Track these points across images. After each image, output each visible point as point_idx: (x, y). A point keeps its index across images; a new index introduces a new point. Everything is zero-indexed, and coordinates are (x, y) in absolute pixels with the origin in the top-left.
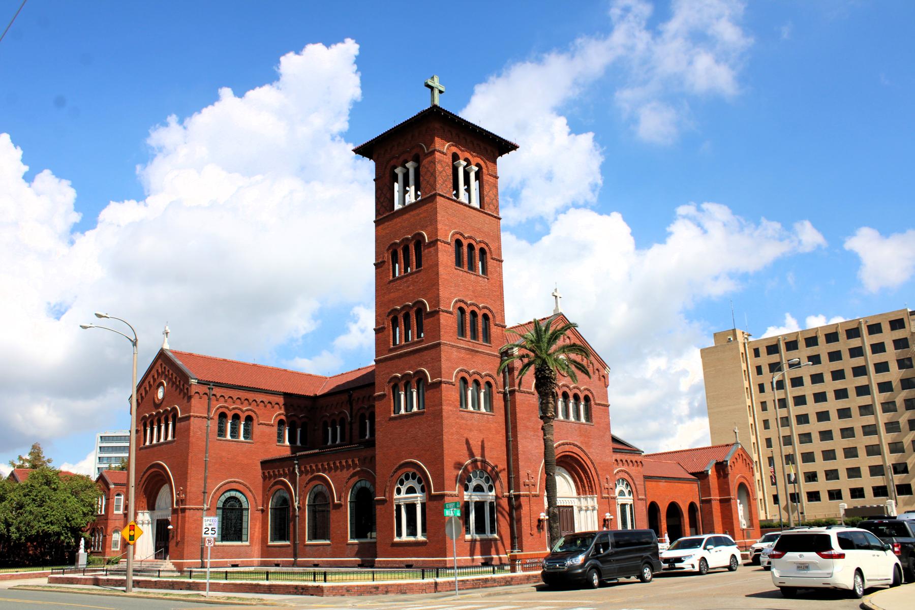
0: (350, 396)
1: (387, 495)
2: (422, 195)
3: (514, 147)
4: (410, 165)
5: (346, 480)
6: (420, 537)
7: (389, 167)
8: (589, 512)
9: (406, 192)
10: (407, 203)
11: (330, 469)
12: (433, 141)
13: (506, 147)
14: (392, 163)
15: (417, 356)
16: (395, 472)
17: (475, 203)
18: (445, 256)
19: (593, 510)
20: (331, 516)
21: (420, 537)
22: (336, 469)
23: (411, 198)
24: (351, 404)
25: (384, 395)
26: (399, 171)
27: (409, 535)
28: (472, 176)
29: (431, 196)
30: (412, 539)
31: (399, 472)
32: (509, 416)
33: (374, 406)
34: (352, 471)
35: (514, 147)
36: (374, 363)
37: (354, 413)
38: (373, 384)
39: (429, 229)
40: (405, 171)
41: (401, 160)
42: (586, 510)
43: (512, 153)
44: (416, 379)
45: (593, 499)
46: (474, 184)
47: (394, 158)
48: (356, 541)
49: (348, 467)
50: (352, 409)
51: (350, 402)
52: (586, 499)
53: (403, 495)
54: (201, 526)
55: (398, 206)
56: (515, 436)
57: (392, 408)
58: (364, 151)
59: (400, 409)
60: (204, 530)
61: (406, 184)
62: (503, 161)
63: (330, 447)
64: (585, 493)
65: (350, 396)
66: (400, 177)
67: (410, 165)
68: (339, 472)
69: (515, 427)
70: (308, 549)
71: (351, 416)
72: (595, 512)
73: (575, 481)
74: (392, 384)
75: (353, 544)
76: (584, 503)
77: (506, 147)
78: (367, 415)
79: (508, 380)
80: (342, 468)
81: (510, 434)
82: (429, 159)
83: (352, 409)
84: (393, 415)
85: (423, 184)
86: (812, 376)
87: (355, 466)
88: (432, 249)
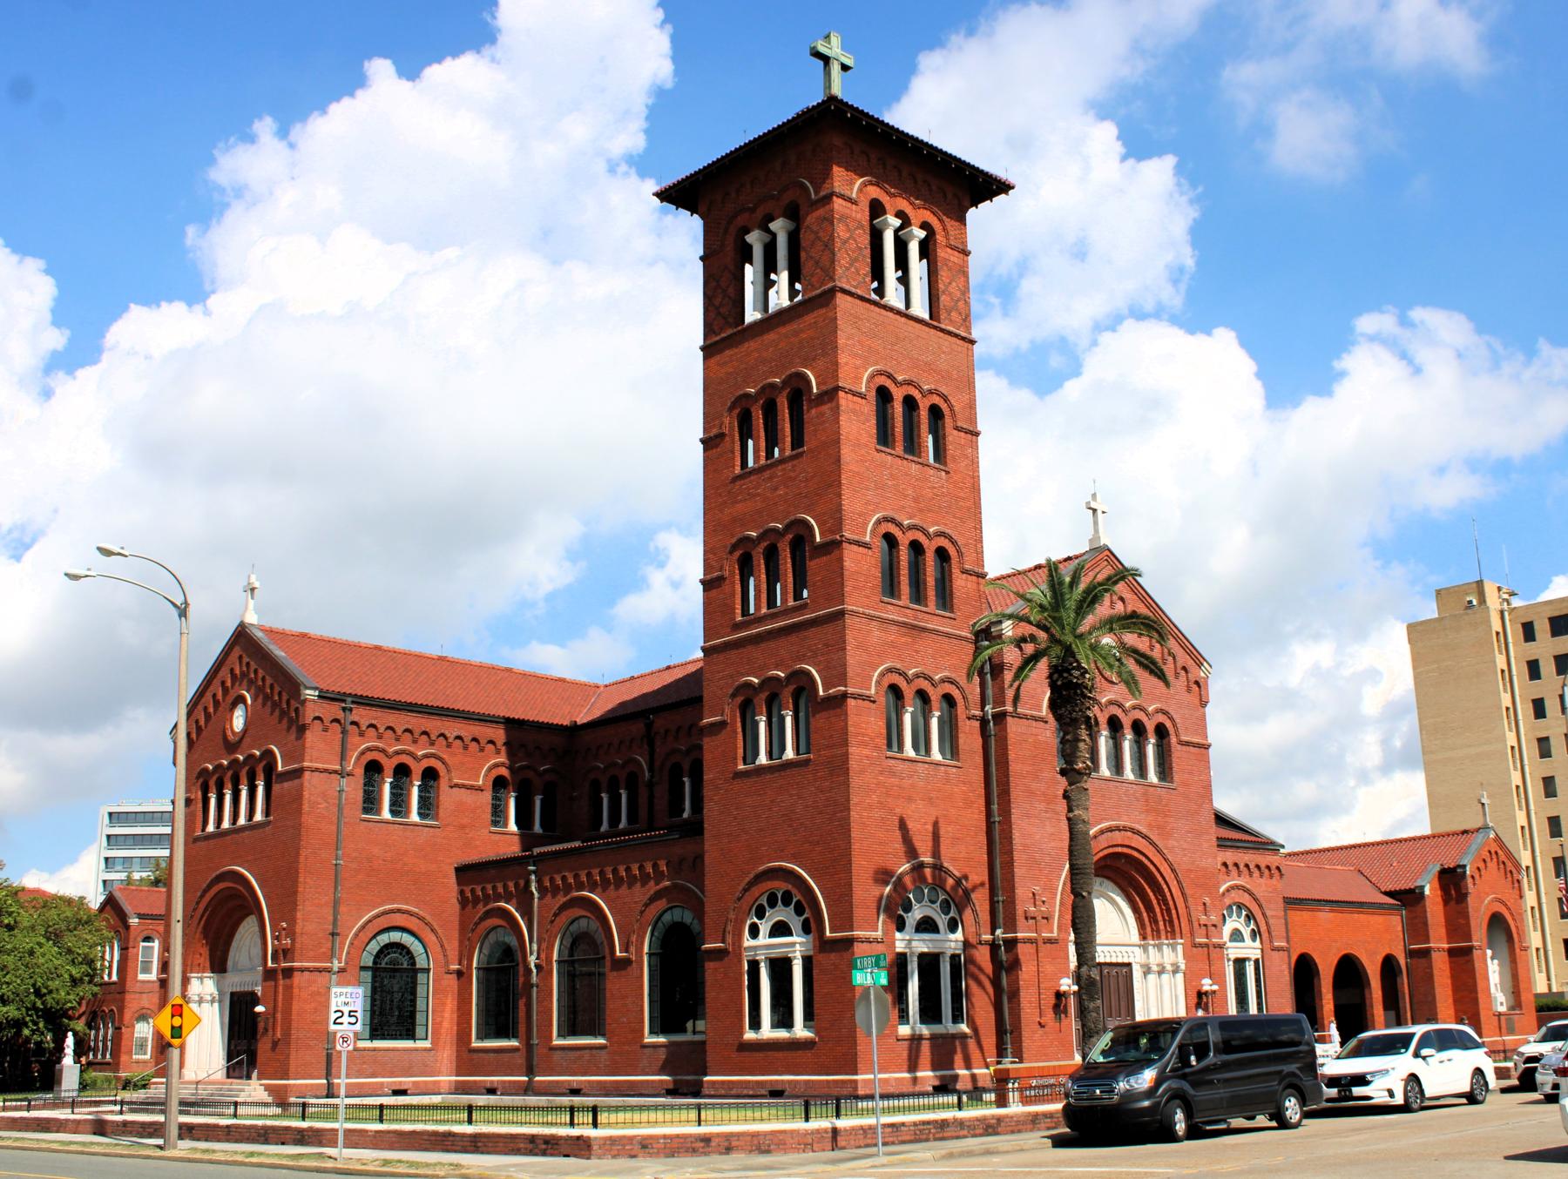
0: (649, 726)
2: (805, 291)
3: (1003, 187)
4: (779, 226)
5: (640, 907)
6: (800, 1031)
7: (733, 230)
8: (1165, 977)
9: (769, 284)
10: (772, 308)
11: (605, 884)
13: (986, 187)
15: (793, 638)
16: (746, 890)
17: (920, 308)
18: (855, 422)
19: (1175, 972)
20: (609, 986)
21: (800, 1031)
22: (619, 882)
23: (780, 298)
25: (723, 724)
26: (755, 239)
28: (914, 249)
29: (824, 293)
30: (782, 1034)
31: (756, 891)
33: (700, 748)
34: (652, 888)
35: (1003, 187)
36: (701, 654)
37: (657, 763)
38: (700, 699)
39: (820, 363)
40: (767, 238)
41: (759, 214)
42: (1160, 973)
43: (1000, 199)
44: (792, 688)
46: (918, 268)
48: (662, 1039)
49: (645, 879)
51: (649, 739)
52: (1159, 947)
53: (763, 939)
55: (752, 315)
56: (1006, 812)
57: (740, 752)
58: (678, 195)
59: (756, 754)
60: (333, 1016)
61: (770, 266)
62: (978, 216)
65: (649, 726)
66: (758, 253)
68: (624, 890)
70: (557, 1055)
71: (651, 770)
72: (1180, 976)
74: (739, 699)
75: (655, 1046)
76: (1154, 957)
77: (986, 187)
78: (686, 766)
79: (990, 692)
82: (821, 212)
85: (807, 267)
87: (659, 876)
88: (826, 408)
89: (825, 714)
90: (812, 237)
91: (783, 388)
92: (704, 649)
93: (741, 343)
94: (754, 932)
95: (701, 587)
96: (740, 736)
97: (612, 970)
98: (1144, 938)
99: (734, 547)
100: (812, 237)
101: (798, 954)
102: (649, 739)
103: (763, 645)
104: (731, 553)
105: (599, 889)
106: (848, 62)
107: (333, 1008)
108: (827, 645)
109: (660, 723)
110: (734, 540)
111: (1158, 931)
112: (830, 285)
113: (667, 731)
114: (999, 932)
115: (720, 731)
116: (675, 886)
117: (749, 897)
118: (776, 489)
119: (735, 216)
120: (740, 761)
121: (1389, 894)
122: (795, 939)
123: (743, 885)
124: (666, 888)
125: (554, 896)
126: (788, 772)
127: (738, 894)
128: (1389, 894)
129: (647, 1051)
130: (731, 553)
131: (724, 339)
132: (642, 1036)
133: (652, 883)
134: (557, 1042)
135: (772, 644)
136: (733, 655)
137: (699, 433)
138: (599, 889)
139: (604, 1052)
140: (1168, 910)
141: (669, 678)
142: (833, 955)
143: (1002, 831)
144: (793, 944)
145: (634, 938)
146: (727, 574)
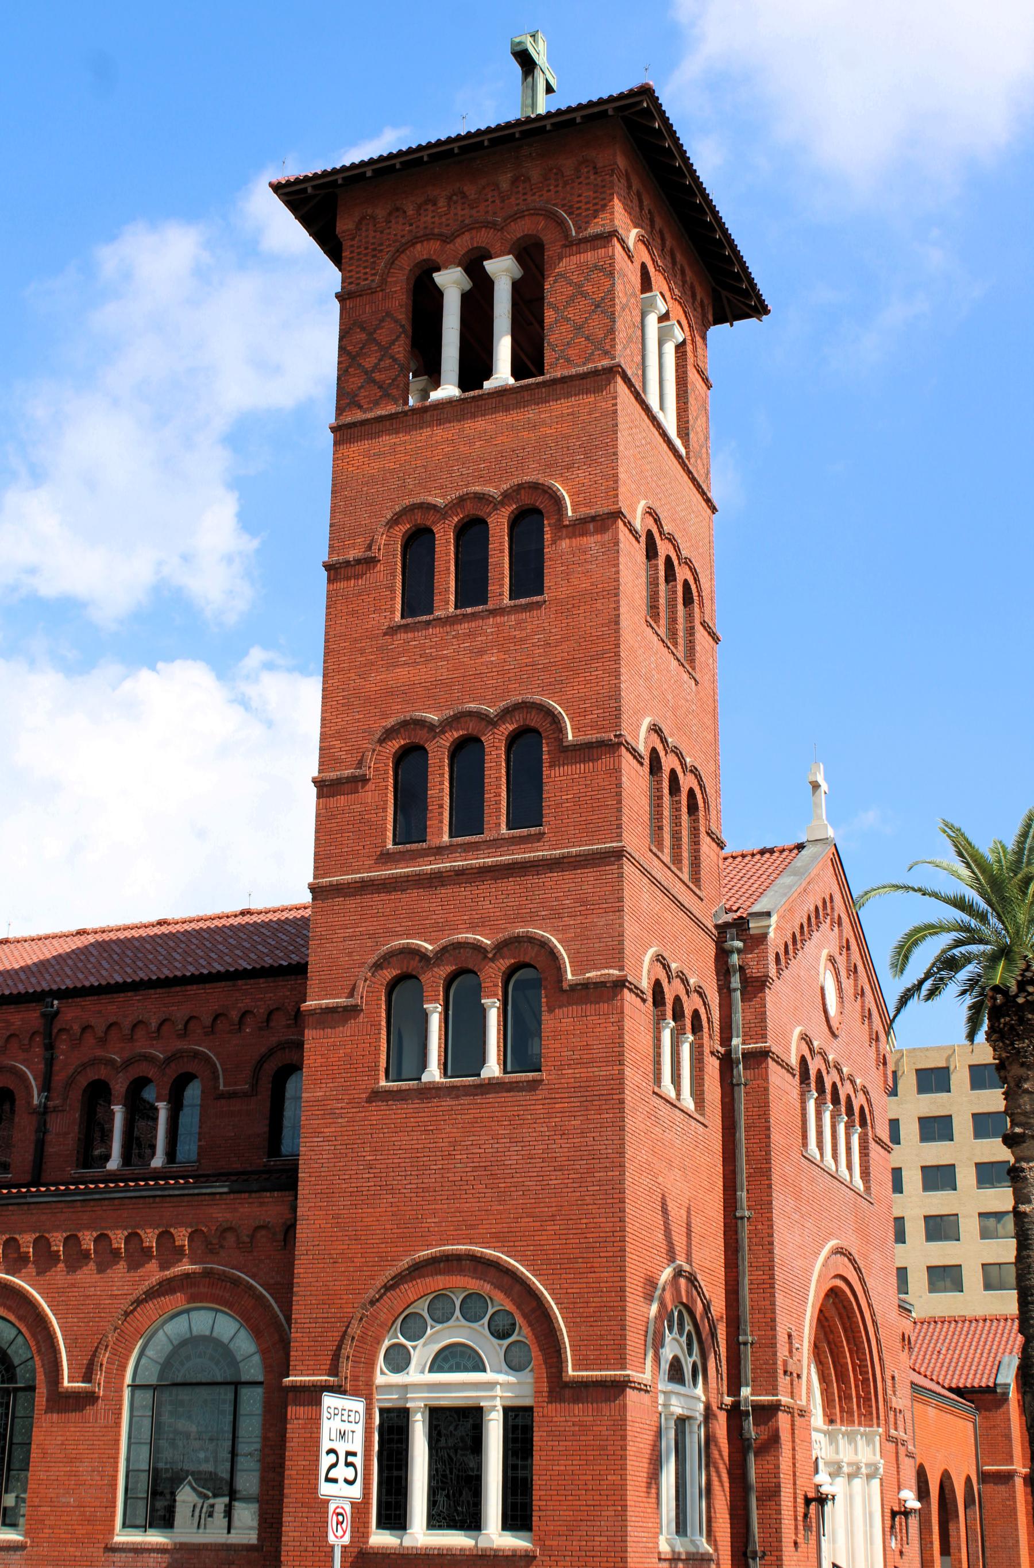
0: (50, 1018)
1: (100, 1377)
5: (125, 1305)
6: (495, 1535)
7: (406, 264)
8: (857, 1482)
11: (46, 1259)
12: (602, 206)
14: (422, 251)
15: (510, 885)
16: (388, 1288)
19: (870, 1477)
20: (37, 1437)
21: (495, 1535)
22: (77, 1258)
24: (50, 1047)
25: (351, 1012)
27: (436, 1520)
29: (595, 373)
30: (456, 1540)
31: (409, 1290)
32: (742, 1135)
33: (300, 1045)
34: (153, 1274)
36: (307, 898)
37: (60, 1078)
38: (300, 970)
39: (581, 475)
41: (463, 244)
42: (851, 1477)
44: (504, 963)
45: (869, 1442)
47: (428, 237)
49: (138, 1256)
50: (50, 1062)
51: (49, 1036)
52: (851, 1437)
53: (416, 1374)
54: (316, 1442)
56: (764, 1205)
57: (383, 1063)
59: (424, 1065)
60: (326, 1461)
63: (157, 1175)
64: (847, 1416)
65: (50, 1018)
67: (502, 269)
68: (87, 1274)
69: (763, 1172)
71: (46, 1086)
72: (876, 1483)
73: (823, 1378)
74: (389, 974)
76: (846, 1453)
78: (119, 1086)
79: (738, 1018)
80: (107, 1257)
81: (743, 1195)
82: (589, 257)
83: (50, 1062)
84: (383, 1083)
86: (922, 1120)
87: (170, 1253)
88: (592, 542)
89: (575, 1010)
90: (570, 290)
91: (502, 503)
92: (313, 889)
93: (378, 434)
94: (399, 1360)
95: (314, 790)
96: (384, 1032)
97: (49, 1409)
98: (832, 1422)
99: (389, 734)
100: (570, 290)
101: (498, 1403)
102: (49, 1036)
103: (443, 891)
104: (381, 741)
105: (31, 1269)
106: (553, 83)
107: (326, 1445)
108: (584, 903)
109: (72, 1014)
110: (390, 722)
111: (850, 1413)
112: (606, 363)
113: (86, 1028)
114: (746, 1391)
115: (345, 1021)
116: (207, 1274)
117: (394, 1300)
118: (481, 652)
119: (412, 243)
120: (382, 1074)
121: (950, 1389)
122: (488, 1376)
123: (379, 1282)
124: (187, 1275)
125: (101, 1269)
126: (491, 1097)
127: (372, 1293)
128: (950, 1389)
129: (117, 1557)
130: (381, 741)
131: (380, 419)
132: (111, 1531)
133: (153, 1265)
134: (122, 1537)
135: (464, 892)
136: (378, 901)
137: (323, 554)
138: (31, 1269)
139: (17, 1556)
140: (866, 1381)
141: (47, 952)
142: (578, 1408)
143: (755, 1232)
144: (491, 1385)
145: (104, 1357)
146: (371, 774)
